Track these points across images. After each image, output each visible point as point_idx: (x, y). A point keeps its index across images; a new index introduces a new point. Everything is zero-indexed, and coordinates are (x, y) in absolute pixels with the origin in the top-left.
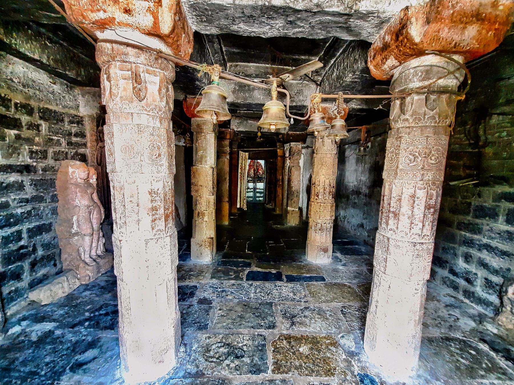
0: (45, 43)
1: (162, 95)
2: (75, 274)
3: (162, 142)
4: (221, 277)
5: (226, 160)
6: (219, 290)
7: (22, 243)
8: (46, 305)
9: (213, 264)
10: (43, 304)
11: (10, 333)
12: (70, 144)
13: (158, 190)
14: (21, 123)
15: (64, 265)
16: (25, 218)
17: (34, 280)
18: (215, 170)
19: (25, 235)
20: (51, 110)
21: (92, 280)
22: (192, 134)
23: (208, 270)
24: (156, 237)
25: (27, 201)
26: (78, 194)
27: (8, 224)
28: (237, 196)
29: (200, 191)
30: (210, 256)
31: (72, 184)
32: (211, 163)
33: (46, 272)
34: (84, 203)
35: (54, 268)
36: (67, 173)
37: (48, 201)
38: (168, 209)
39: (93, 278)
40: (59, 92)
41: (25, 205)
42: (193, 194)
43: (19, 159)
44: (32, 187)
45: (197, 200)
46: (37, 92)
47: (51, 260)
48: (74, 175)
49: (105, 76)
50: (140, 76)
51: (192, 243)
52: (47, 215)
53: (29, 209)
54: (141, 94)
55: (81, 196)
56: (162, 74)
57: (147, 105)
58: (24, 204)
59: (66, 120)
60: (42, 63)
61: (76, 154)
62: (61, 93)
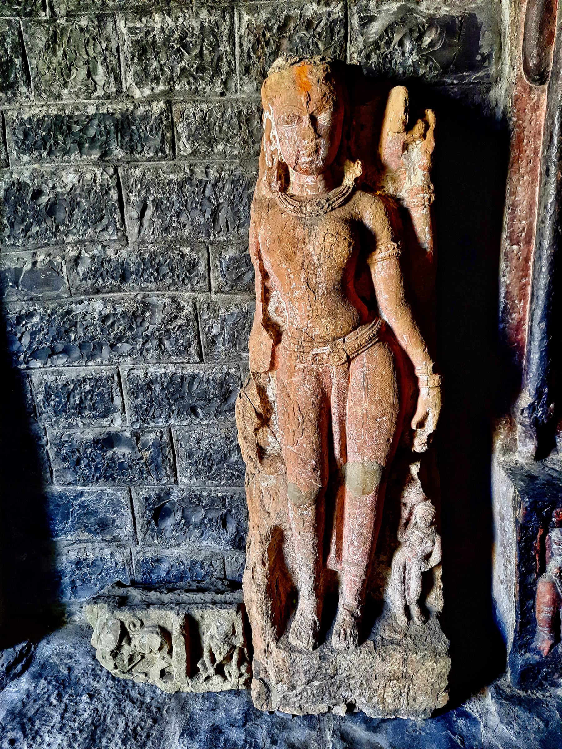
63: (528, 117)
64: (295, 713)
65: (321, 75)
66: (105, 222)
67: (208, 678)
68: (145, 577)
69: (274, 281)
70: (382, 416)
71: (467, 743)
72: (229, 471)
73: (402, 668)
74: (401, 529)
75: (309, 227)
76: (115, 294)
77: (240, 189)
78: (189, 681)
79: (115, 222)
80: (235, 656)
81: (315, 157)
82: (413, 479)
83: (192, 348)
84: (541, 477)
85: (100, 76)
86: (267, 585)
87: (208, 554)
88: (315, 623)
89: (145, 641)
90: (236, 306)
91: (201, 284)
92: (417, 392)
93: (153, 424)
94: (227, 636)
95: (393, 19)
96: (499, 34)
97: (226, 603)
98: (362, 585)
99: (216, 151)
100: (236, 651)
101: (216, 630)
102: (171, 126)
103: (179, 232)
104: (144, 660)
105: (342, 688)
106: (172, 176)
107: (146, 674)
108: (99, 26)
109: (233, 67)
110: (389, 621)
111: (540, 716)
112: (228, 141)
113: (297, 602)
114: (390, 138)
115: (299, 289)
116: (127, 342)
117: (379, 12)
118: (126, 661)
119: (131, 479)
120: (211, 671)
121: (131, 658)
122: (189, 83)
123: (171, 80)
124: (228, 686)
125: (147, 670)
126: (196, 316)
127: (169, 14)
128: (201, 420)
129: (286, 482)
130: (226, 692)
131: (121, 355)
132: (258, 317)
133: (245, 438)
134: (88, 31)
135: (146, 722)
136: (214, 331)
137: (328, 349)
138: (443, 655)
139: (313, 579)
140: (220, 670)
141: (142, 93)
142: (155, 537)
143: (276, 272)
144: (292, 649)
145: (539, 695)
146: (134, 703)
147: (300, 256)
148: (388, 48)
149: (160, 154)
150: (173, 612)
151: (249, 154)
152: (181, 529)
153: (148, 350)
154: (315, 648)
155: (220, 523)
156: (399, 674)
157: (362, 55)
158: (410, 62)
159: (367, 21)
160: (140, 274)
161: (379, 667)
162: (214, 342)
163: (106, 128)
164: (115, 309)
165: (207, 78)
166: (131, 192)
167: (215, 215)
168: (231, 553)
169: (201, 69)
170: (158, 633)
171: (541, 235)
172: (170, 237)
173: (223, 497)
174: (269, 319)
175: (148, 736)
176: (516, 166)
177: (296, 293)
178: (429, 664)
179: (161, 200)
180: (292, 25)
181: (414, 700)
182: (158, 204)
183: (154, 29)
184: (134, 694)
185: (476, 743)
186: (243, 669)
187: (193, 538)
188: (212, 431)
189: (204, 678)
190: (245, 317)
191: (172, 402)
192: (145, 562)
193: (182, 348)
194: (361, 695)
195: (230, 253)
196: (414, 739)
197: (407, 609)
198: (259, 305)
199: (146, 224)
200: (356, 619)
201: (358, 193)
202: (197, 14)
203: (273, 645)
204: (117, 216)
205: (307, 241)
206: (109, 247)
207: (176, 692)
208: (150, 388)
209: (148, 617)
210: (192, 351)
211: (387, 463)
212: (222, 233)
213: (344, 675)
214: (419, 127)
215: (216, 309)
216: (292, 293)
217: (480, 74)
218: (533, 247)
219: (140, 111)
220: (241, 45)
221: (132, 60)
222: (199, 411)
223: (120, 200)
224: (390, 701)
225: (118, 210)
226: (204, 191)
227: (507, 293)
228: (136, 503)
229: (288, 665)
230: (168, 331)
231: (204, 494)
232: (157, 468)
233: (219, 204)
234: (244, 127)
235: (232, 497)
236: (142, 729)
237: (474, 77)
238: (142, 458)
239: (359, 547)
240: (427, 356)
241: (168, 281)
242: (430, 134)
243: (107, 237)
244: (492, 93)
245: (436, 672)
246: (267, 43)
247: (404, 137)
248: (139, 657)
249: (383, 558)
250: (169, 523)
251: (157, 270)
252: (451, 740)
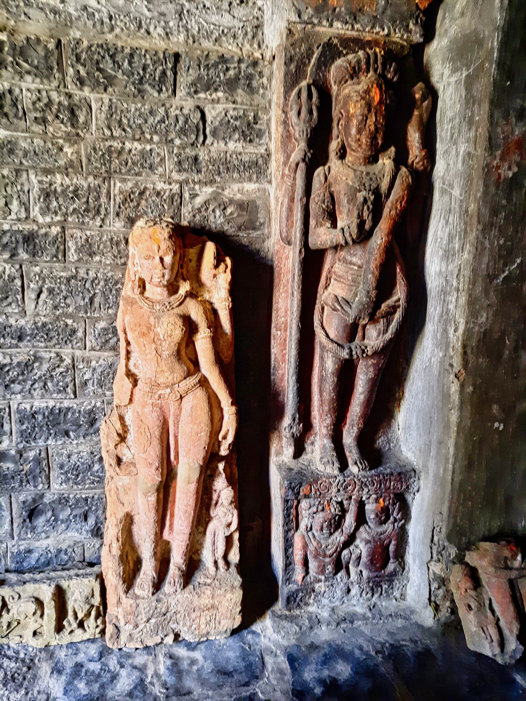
63: (283, 263)
64: (137, 647)
65: (166, 235)
66: (10, 300)
67: (72, 632)
68: (18, 565)
69: (133, 347)
70: (201, 433)
71: (252, 649)
72: (91, 477)
73: (211, 601)
74: (212, 507)
75: (158, 318)
76: (13, 350)
77: (110, 285)
78: (57, 636)
79: (18, 301)
80: (93, 613)
81: (162, 279)
82: (220, 473)
83: (69, 388)
84: (296, 469)
85: (15, 206)
86: (120, 555)
87: (72, 543)
88: (154, 578)
89: (21, 609)
90: (104, 360)
91: (78, 344)
92: (222, 418)
93: (33, 444)
94: (87, 598)
95: (209, 197)
96: (269, 212)
97: (87, 574)
98: (187, 548)
99: (94, 260)
100: (94, 609)
101: (79, 595)
102: (65, 242)
103: (65, 309)
104: (19, 626)
105: (171, 622)
106: (62, 274)
107: (21, 637)
108: (17, 176)
109: (108, 211)
110: (205, 572)
111: (297, 625)
112: (103, 255)
113: (141, 566)
114: (206, 271)
115: (151, 354)
116: (19, 383)
117: (201, 192)
118: (5, 627)
119: (13, 487)
120: (75, 625)
121: (9, 625)
122: (78, 217)
123: (66, 215)
124: (87, 636)
125: (21, 634)
126: (74, 366)
127: (67, 175)
128: (73, 440)
129: (136, 480)
130: (85, 641)
131: (13, 393)
132: (121, 370)
133: (107, 451)
134: (8, 178)
135: (21, 670)
136: (86, 377)
137: (168, 390)
138: (237, 588)
139: (153, 546)
140: (81, 625)
141: (44, 220)
142: (29, 532)
143: (136, 343)
144: (137, 597)
145: (298, 612)
146: (10, 659)
147: (152, 335)
148: (207, 212)
149: (55, 259)
150: (45, 585)
151: (117, 264)
152: (51, 524)
153: (35, 390)
154: (153, 594)
155: (83, 517)
156: (209, 606)
157: (191, 214)
158: (219, 222)
159: (194, 196)
160: (33, 336)
161: (196, 602)
162: (86, 384)
163: (16, 238)
164: (12, 360)
165: (91, 216)
166: (31, 281)
167: (91, 300)
168: (90, 541)
169: (87, 210)
170: (32, 602)
171: (291, 328)
172: (58, 313)
173: (86, 498)
174: (129, 371)
175: (24, 679)
176: (278, 288)
177: (149, 356)
178: (229, 596)
179: (53, 289)
180: (148, 193)
181: (219, 623)
182: (51, 291)
183: (56, 183)
184: (10, 653)
185: (258, 647)
186: (99, 621)
187: (59, 532)
188: (81, 448)
189: (69, 631)
190: (110, 368)
191: (50, 427)
192: (19, 553)
193: (62, 389)
194: (184, 625)
195: (102, 325)
196: (218, 651)
197: (216, 562)
198: (123, 361)
199: (41, 302)
200: (182, 571)
201: (188, 299)
202: (86, 179)
203: (123, 596)
204: (19, 297)
205: (156, 326)
206: (11, 317)
207: (46, 646)
208: (34, 417)
209: (24, 591)
210: (69, 390)
211: (204, 462)
212: (96, 312)
213: (173, 611)
214: (222, 266)
215: (89, 362)
216: (146, 355)
217: (259, 232)
218: (288, 333)
219: (43, 231)
220: (115, 200)
221: (39, 199)
222: (71, 434)
223: (23, 286)
224: (203, 626)
225: (20, 293)
226: (85, 285)
227: (275, 358)
228: (15, 506)
229: (134, 609)
230: (52, 376)
231: (71, 496)
232: (34, 477)
233: (95, 294)
234: (115, 247)
235: (93, 497)
236: (19, 674)
237: (254, 234)
238: (23, 470)
239: (185, 521)
240: (228, 396)
241: (54, 341)
242: (228, 271)
243: (10, 310)
244: (266, 243)
245: (233, 601)
246: (132, 201)
247: (214, 271)
248: (16, 623)
249: (201, 529)
250: (40, 521)
251: (47, 334)
252: (242, 647)
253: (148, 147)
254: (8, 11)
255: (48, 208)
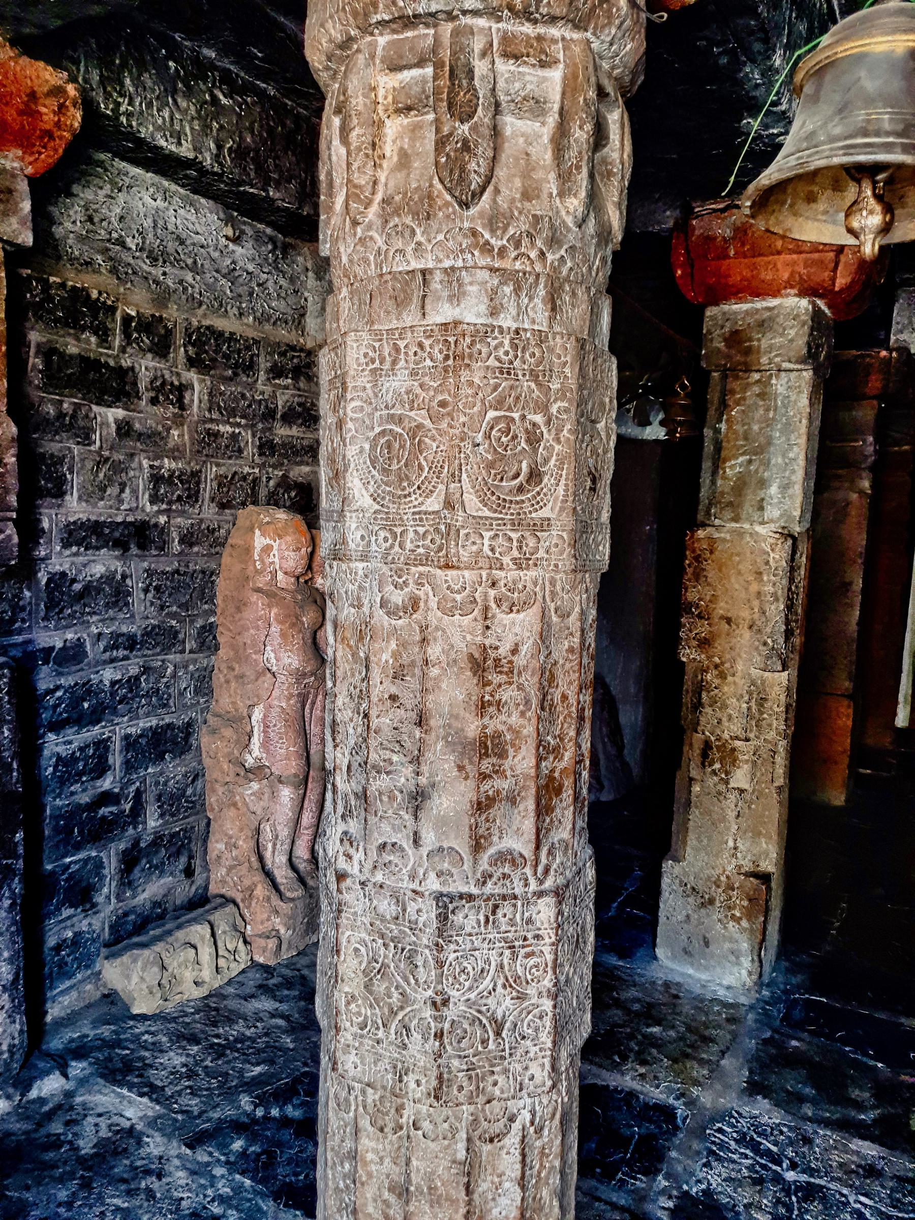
0: (213, 96)
1: (572, 155)
2: (239, 920)
3: (554, 409)
4: (801, 1099)
5: (854, 496)
6: (790, 1176)
7: (107, 783)
8: (143, 1017)
9: (763, 1009)
10: (136, 1011)
11: (33, 1094)
12: (266, 447)
13: (515, 651)
14: (135, 384)
15: (212, 876)
16: (120, 702)
17: (126, 914)
18: (804, 548)
19: (116, 759)
20: (221, 334)
21: (285, 955)
22: (701, 380)
23: (735, 1036)
24: (489, 888)
25: (131, 643)
26: (273, 629)
27: (75, 716)
28: (900, 671)
29: (720, 645)
30: (746, 962)
31: (258, 590)
32: (785, 514)
33: (162, 892)
34: (287, 661)
35: (187, 883)
36: (248, 550)
37: (188, 647)
38: (556, 751)
39: (289, 948)
40: (250, 267)
41: (126, 658)
42: (688, 654)
43: (121, 502)
44: (150, 596)
45: (700, 687)
46: (189, 277)
47: (178, 853)
48: (268, 561)
49: (336, 121)
50: (470, 74)
51: (666, 881)
52: (181, 694)
53: (134, 671)
54: (473, 166)
55: (283, 635)
56: (577, 50)
57: (495, 221)
58: (121, 653)
59: (264, 363)
60: (202, 171)
61: (285, 483)
62: (257, 271)
253: (237, 431)
254: (118, 278)
255: (156, 494)
